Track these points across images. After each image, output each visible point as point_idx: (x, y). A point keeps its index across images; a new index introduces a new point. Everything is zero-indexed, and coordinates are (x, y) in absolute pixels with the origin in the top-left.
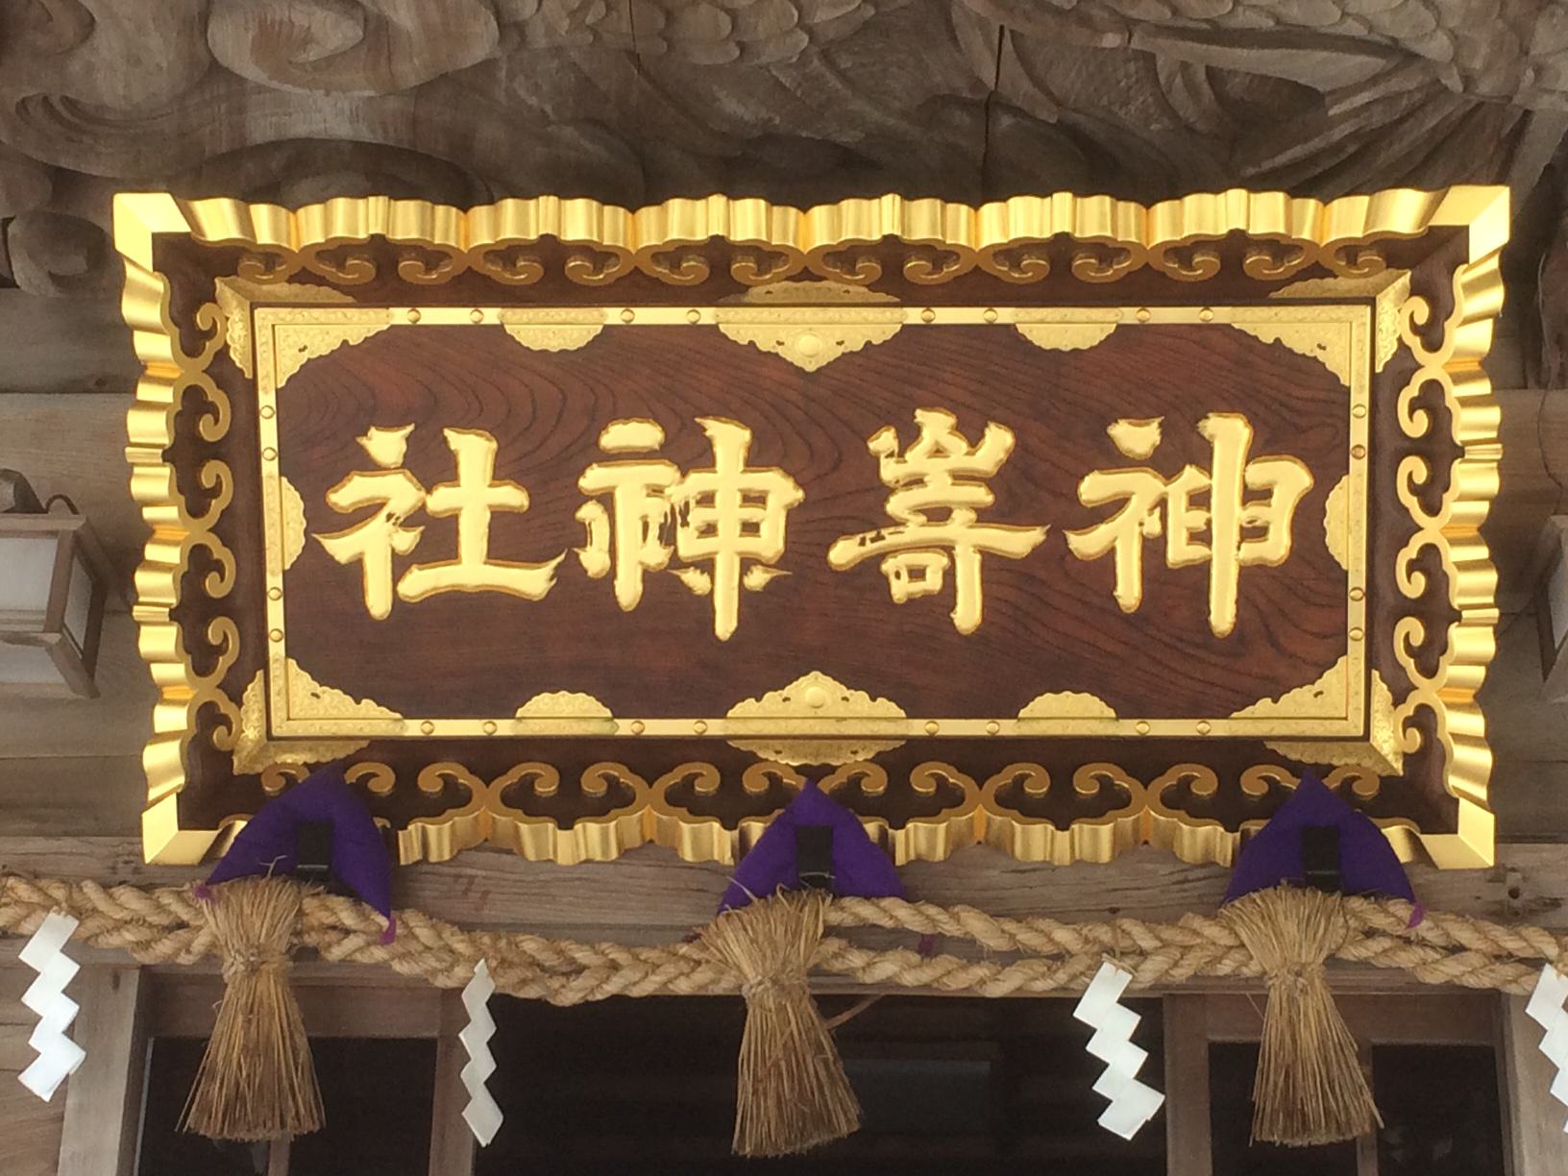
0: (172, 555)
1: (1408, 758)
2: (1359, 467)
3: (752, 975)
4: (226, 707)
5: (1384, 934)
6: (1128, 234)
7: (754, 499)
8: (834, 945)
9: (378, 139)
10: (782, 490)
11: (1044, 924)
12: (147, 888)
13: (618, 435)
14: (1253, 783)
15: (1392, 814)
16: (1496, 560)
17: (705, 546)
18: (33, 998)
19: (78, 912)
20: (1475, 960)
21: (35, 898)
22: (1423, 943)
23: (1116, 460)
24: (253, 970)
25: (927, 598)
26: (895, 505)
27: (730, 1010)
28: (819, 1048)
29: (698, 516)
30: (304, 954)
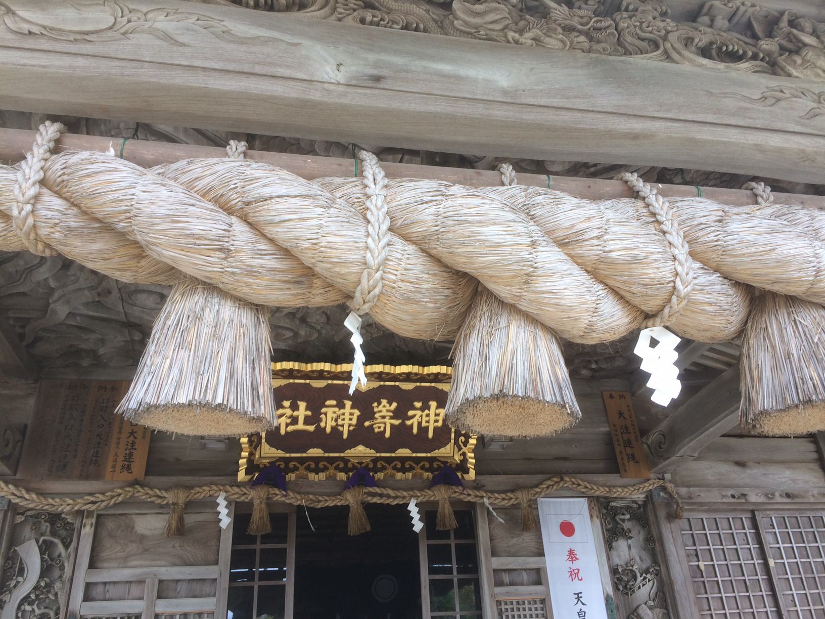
1: (460, 461)
3: (351, 501)
5: (457, 492)
6: (333, 370)
7: (352, 414)
8: (365, 496)
9: (290, 349)
10: (357, 413)
11: (401, 491)
13: (328, 403)
14: (435, 465)
15: (458, 471)
17: (343, 422)
18: (219, 509)
19: (226, 492)
21: (217, 489)
22: (464, 494)
23: (414, 408)
25: (381, 432)
26: (377, 415)
27: (347, 508)
28: (364, 515)
29: (342, 417)
30: (268, 498)
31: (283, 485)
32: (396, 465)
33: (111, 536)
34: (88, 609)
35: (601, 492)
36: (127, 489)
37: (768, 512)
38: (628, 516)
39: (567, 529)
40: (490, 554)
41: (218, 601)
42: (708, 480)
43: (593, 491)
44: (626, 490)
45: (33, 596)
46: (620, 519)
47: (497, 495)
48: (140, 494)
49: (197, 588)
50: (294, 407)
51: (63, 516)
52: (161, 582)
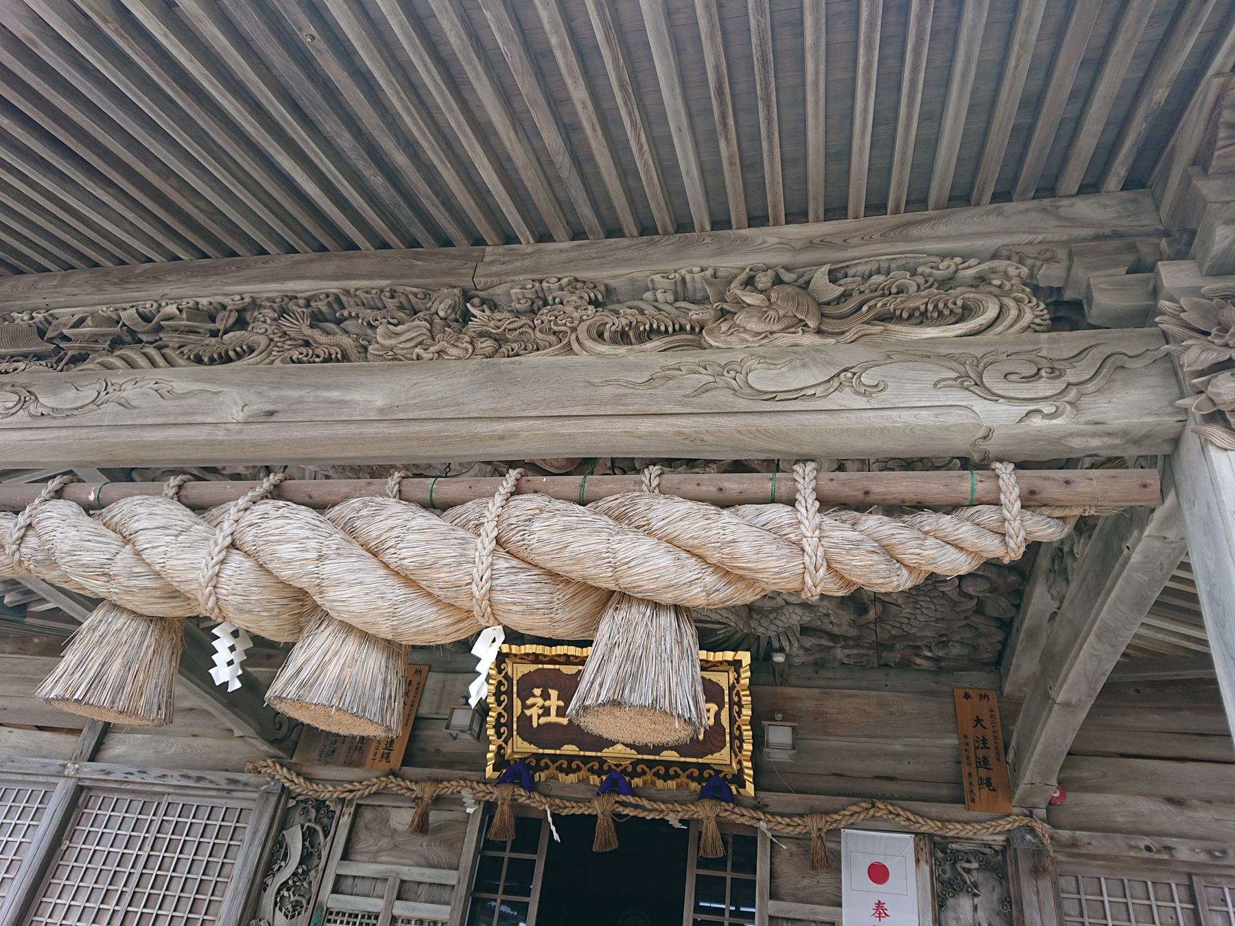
0: (494, 714)
2: (727, 706)
4: (504, 745)
8: (617, 805)
12: (485, 784)
16: (752, 729)
20: (747, 818)
24: (502, 804)
31: (531, 786)
32: (561, 764)
33: (367, 828)
34: (335, 902)
35: (928, 827)
36: (382, 779)
37: (1217, 880)
38: (975, 865)
39: (878, 873)
40: (767, 896)
41: (451, 914)
42: (1116, 822)
43: (917, 825)
44: (968, 827)
45: (290, 882)
46: (964, 869)
47: (779, 819)
48: (393, 785)
49: (437, 893)
50: (545, 696)
51: (327, 803)
52: (403, 882)
